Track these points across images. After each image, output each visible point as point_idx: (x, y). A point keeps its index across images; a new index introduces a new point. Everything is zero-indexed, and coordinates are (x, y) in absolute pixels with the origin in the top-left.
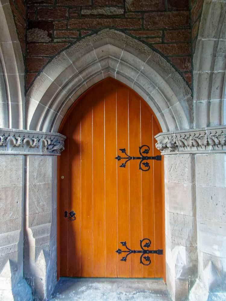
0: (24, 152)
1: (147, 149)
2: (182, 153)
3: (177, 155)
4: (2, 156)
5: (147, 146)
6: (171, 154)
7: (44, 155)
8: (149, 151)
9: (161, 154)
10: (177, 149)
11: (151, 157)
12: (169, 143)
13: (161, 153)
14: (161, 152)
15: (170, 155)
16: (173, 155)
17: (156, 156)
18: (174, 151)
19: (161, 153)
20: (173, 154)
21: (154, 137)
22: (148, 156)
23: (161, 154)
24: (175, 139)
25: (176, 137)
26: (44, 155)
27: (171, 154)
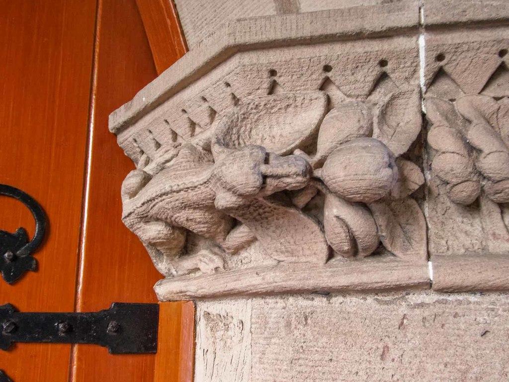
0: (368, 49)
1: (24, 233)
2: (472, 277)
3: (415, 298)
4: (503, 14)
5: (27, 199)
6: (327, 293)
7: (491, 153)
8: (42, 257)
9: (162, 290)
10: (422, 223)
11: (60, 317)
12: (145, 172)
13: (159, 277)
14: (162, 266)
15: (319, 302)
16: (352, 302)
17: (103, 303)
18: (379, 251)
19: (159, 277)
20: (365, 291)
21: (102, 122)
22: (24, 308)
23: (162, 290)
24: (415, 97)
25: (439, 75)
26: (491, 153)
27: (327, 293)
